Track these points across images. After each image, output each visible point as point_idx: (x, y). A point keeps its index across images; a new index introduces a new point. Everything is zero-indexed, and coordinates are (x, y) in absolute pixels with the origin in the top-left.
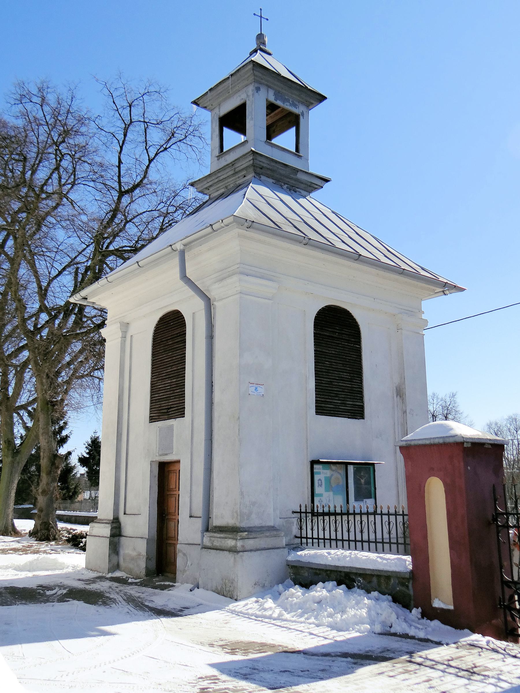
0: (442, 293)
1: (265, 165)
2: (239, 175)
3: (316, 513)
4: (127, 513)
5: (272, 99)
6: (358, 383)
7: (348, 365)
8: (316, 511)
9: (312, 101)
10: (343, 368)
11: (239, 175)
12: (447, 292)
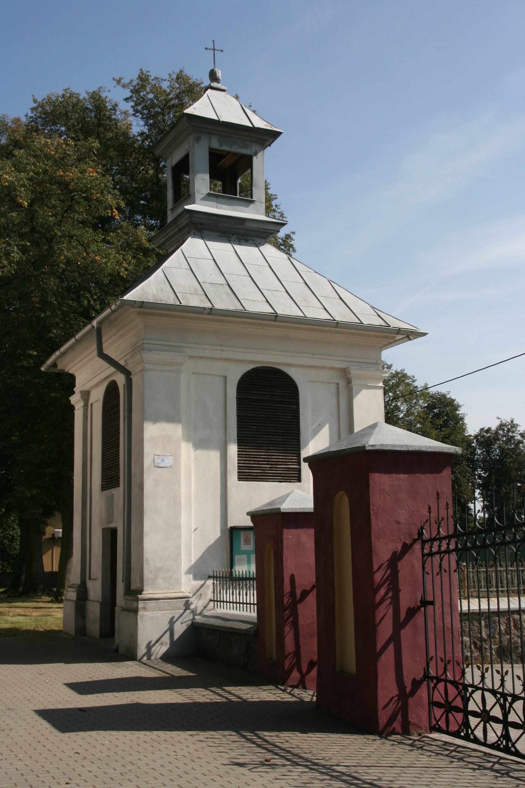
0: (407, 339)
1: (204, 221)
2: (184, 231)
3: (234, 578)
4: (92, 578)
5: (215, 144)
6: (293, 445)
7: (280, 427)
8: (234, 576)
9: (267, 138)
10: (274, 431)
11: (184, 231)
12: (411, 337)
